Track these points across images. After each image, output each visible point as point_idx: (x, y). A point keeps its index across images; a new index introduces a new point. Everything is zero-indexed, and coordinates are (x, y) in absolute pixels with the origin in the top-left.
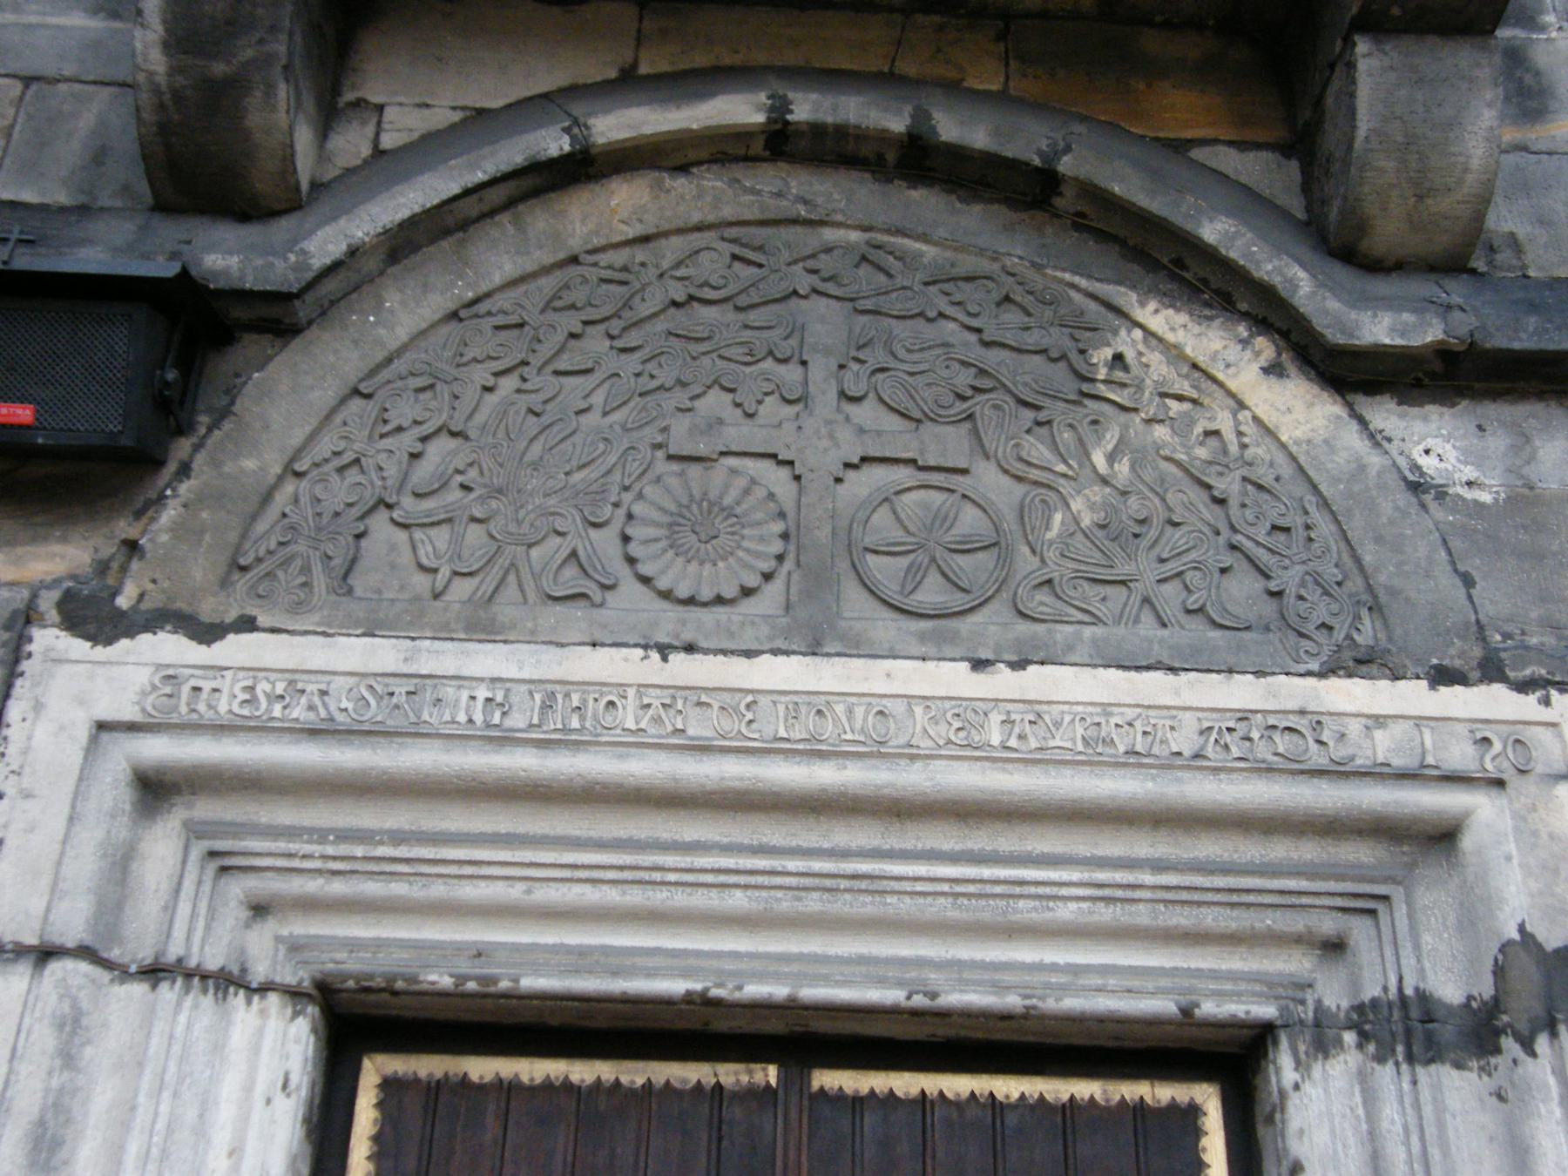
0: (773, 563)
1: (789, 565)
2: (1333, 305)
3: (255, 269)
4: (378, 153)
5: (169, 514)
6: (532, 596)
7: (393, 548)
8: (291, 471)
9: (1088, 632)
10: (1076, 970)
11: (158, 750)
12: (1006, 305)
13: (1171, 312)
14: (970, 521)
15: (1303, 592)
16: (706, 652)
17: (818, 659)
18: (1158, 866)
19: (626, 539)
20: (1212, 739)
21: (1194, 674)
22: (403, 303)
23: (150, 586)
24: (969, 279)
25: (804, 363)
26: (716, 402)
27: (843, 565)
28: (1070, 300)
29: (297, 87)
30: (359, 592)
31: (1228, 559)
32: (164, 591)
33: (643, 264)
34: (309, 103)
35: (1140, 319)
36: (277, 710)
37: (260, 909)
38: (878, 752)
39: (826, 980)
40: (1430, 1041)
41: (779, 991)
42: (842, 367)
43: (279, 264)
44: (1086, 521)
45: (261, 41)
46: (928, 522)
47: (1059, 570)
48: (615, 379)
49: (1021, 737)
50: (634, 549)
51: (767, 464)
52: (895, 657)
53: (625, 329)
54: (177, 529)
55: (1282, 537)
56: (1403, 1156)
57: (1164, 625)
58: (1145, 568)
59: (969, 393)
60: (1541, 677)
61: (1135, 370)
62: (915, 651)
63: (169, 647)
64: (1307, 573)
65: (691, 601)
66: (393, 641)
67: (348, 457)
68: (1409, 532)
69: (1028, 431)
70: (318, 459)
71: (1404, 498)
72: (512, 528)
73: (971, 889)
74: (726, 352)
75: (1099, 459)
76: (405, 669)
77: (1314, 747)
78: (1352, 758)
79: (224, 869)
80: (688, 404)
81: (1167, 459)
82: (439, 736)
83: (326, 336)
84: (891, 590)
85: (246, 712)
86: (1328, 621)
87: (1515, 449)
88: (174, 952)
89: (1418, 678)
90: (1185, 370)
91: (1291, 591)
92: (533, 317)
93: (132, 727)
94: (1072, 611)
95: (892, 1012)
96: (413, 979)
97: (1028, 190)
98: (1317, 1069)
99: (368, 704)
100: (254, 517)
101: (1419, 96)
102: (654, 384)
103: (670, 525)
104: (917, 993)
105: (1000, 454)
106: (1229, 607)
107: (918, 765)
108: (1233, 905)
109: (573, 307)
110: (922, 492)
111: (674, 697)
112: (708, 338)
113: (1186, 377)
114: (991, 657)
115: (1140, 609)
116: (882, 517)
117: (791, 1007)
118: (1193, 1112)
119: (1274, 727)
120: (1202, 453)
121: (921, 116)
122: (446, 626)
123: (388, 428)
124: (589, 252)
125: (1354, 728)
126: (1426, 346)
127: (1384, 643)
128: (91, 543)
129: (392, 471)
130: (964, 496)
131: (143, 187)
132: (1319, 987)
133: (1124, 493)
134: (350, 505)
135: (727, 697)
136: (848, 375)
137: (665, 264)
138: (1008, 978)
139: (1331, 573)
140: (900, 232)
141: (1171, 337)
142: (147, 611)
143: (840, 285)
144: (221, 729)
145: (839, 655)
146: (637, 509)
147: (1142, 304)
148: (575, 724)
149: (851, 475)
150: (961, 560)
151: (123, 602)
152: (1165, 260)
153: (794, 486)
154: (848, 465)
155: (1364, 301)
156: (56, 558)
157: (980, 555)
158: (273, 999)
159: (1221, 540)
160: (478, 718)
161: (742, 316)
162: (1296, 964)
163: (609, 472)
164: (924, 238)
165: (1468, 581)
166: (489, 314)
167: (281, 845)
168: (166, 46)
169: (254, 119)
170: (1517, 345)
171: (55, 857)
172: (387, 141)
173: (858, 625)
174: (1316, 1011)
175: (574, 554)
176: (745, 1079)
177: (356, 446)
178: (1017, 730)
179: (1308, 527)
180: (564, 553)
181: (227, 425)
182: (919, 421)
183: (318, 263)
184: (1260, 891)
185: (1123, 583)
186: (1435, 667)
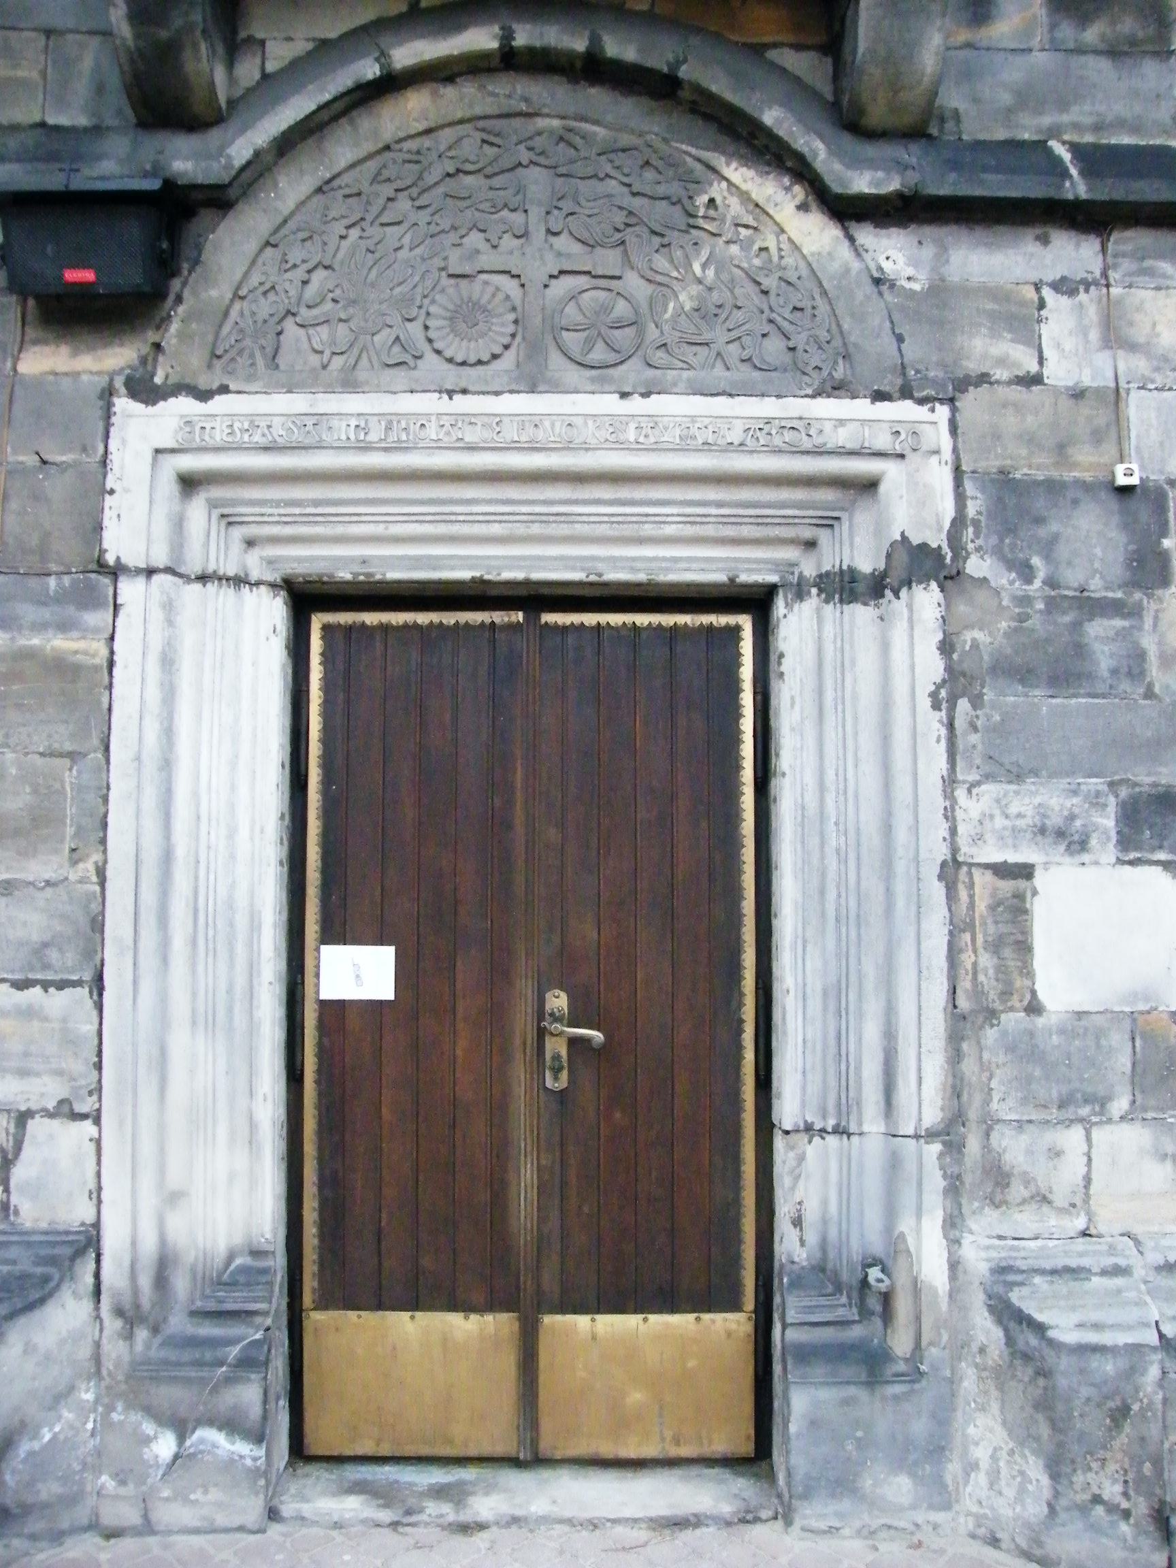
1: (519, 338)
2: (837, 166)
4: (265, 76)
5: (174, 327)
6: (376, 365)
8: (236, 296)
9: (685, 374)
10: (675, 560)
12: (646, 168)
14: (621, 309)
15: (807, 348)
18: (720, 504)
19: (426, 328)
23: (170, 370)
24: (624, 150)
25: (526, 211)
26: (475, 239)
28: (685, 162)
29: (212, 45)
30: (282, 367)
31: (767, 328)
33: (429, 149)
34: (220, 49)
35: (726, 175)
36: (246, 438)
37: (250, 543)
38: (568, 447)
39: (544, 569)
40: (852, 591)
41: (520, 575)
42: (548, 213)
43: (215, 165)
44: (687, 308)
47: (671, 337)
49: (646, 436)
50: (431, 334)
52: (577, 392)
53: (419, 194)
54: (181, 335)
55: (798, 314)
56: (832, 648)
57: (728, 369)
58: (719, 335)
61: (721, 210)
62: (589, 388)
65: (464, 363)
67: (267, 286)
69: (657, 251)
71: (869, 288)
73: (620, 519)
74: (481, 207)
77: (805, 438)
78: (825, 444)
79: (230, 524)
80: (459, 241)
81: (738, 267)
82: (332, 448)
83: (246, 208)
84: (576, 353)
87: (937, 257)
88: (211, 568)
90: (751, 207)
91: (800, 348)
92: (365, 187)
93: (173, 451)
95: (580, 584)
96: (331, 576)
97: (659, 87)
98: (796, 606)
100: (220, 326)
102: (439, 229)
103: (451, 319)
107: (590, 453)
108: (758, 524)
109: (389, 180)
111: (457, 421)
112: (470, 197)
113: (751, 212)
116: (571, 309)
117: (527, 583)
118: (734, 632)
120: (757, 262)
121: (595, 40)
122: (330, 385)
123: (289, 266)
125: (828, 427)
126: (891, 193)
127: (850, 378)
129: (293, 293)
130: (618, 293)
131: (129, 112)
133: (710, 289)
134: (271, 315)
135: (486, 419)
136: (551, 218)
137: (442, 148)
138: (639, 565)
139: (824, 336)
140: (583, 119)
141: (744, 187)
143: (547, 157)
144: (217, 449)
146: (433, 309)
147: (728, 165)
148: (404, 437)
149: (553, 282)
150: (617, 333)
152: (745, 133)
154: (551, 276)
155: (856, 163)
156: (118, 356)
157: (627, 330)
158: (263, 588)
159: (764, 316)
160: (352, 437)
161: (488, 181)
162: (789, 554)
163: (415, 287)
164: (596, 122)
165: (900, 339)
166: (340, 187)
167: (257, 510)
169: (190, 66)
170: (942, 192)
172: (270, 67)
175: (398, 338)
176: (506, 619)
177: (273, 278)
178: (644, 433)
179: (814, 308)
181: (199, 269)
182: (592, 246)
183: (238, 162)
184: (773, 517)
185: (707, 344)
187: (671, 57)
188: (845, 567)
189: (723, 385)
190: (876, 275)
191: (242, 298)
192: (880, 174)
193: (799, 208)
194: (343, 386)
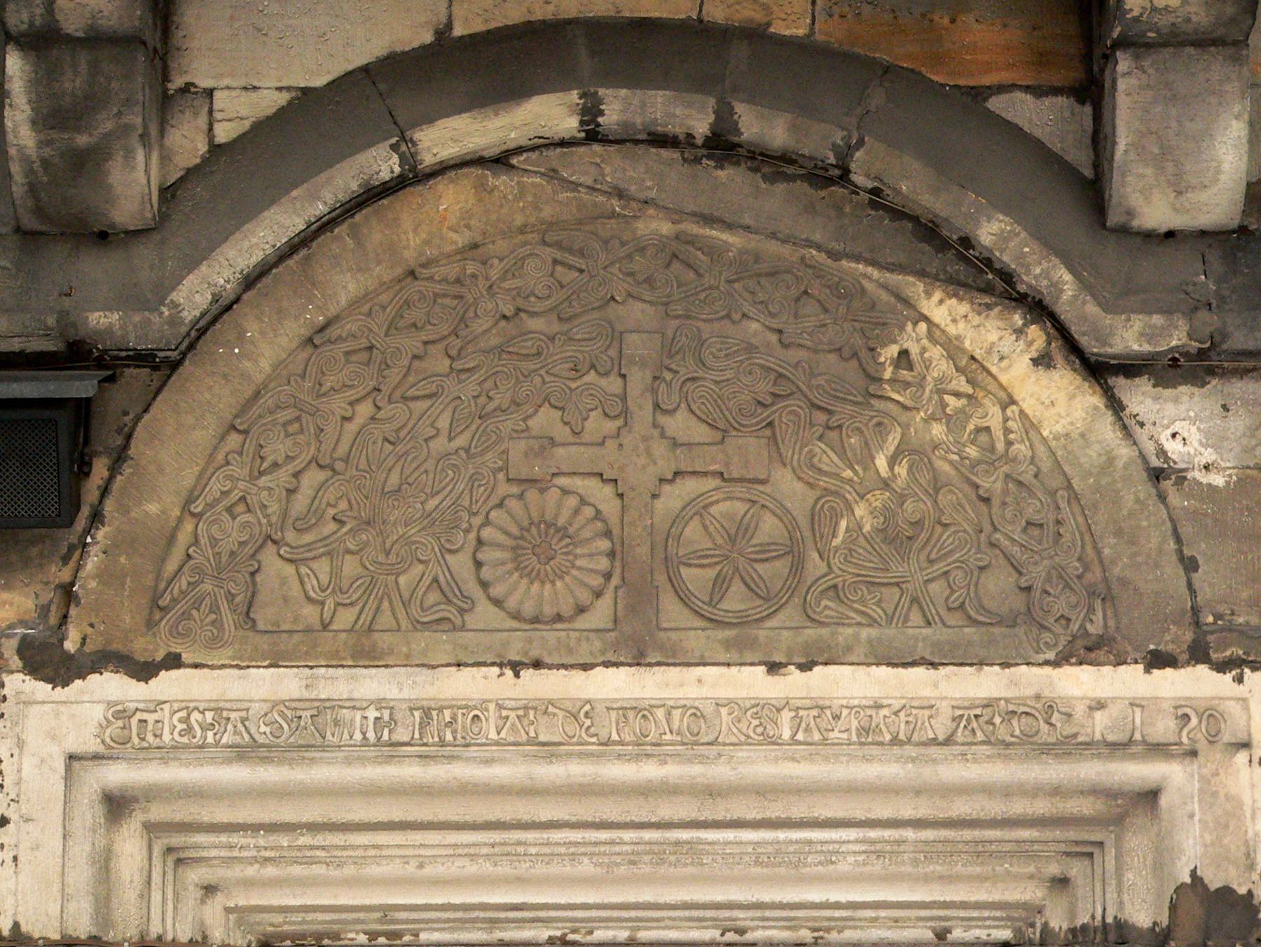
0: (600, 580)
1: (615, 580)
2: (1092, 309)
3: (135, 326)
6: (404, 624)
7: (283, 581)
9: (865, 633)
11: (118, 775)
13: (954, 301)
14: (769, 527)
16: (550, 667)
17: (642, 669)
18: (918, 824)
19: (478, 564)
20: (962, 725)
21: (951, 668)
22: (262, 333)
23: (89, 630)
25: (624, 376)
26: (545, 420)
27: (661, 578)
28: (863, 290)
30: (261, 626)
32: (101, 633)
33: (474, 276)
42: (656, 378)
43: (155, 319)
45: (120, 114)
46: (733, 532)
48: (458, 402)
50: (486, 573)
51: (594, 483)
52: (705, 664)
54: (104, 575)
59: (769, 400)
60: (1239, 658)
61: (918, 367)
62: (722, 659)
63: (111, 686)
64: (1054, 568)
65: (536, 620)
66: (295, 670)
67: (236, 495)
68: (1145, 523)
70: (209, 499)
71: (1144, 488)
72: (381, 558)
75: (881, 463)
76: (306, 695)
77: (1044, 728)
78: (1075, 735)
85: (185, 740)
86: (1066, 613)
89: (1136, 662)
91: (1038, 585)
94: (852, 614)
99: (281, 727)
101: (1174, 111)
103: (514, 549)
104: (729, 931)
105: (795, 463)
106: (985, 602)
110: (728, 503)
114: (783, 661)
115: (909, 609)
119: (1013, 712)
122: (336, 654)
124: (422, 266)
125: (1080, 710)
128: (32, 589)
129: (274, 508)
130: (763, 506)
132: (1047, 913)
140: (709, 220)
142: (90, 654)
145: (659, 664)
146: (487, 533)
147: (929, 295)
149: (667, 488)
151: (70, 646)
153: (618, 502)
164: (730, 227)
165: (1190, 565)
167: (223, 838)
168: (34, 123)
171: (59, 869)
172: (223, 133)
173: (674, 636)
174: (1042, 932)
179: (1058, 522)
180: (427, 581)
186: (1151, 652)
187: (838, 137)
188: (1109, 920)
189: (923, 651)
190: (1155, 462)
191: (198, 516)
192: (1157, 319)
193: (1036, 362)
194: (353, 657)
